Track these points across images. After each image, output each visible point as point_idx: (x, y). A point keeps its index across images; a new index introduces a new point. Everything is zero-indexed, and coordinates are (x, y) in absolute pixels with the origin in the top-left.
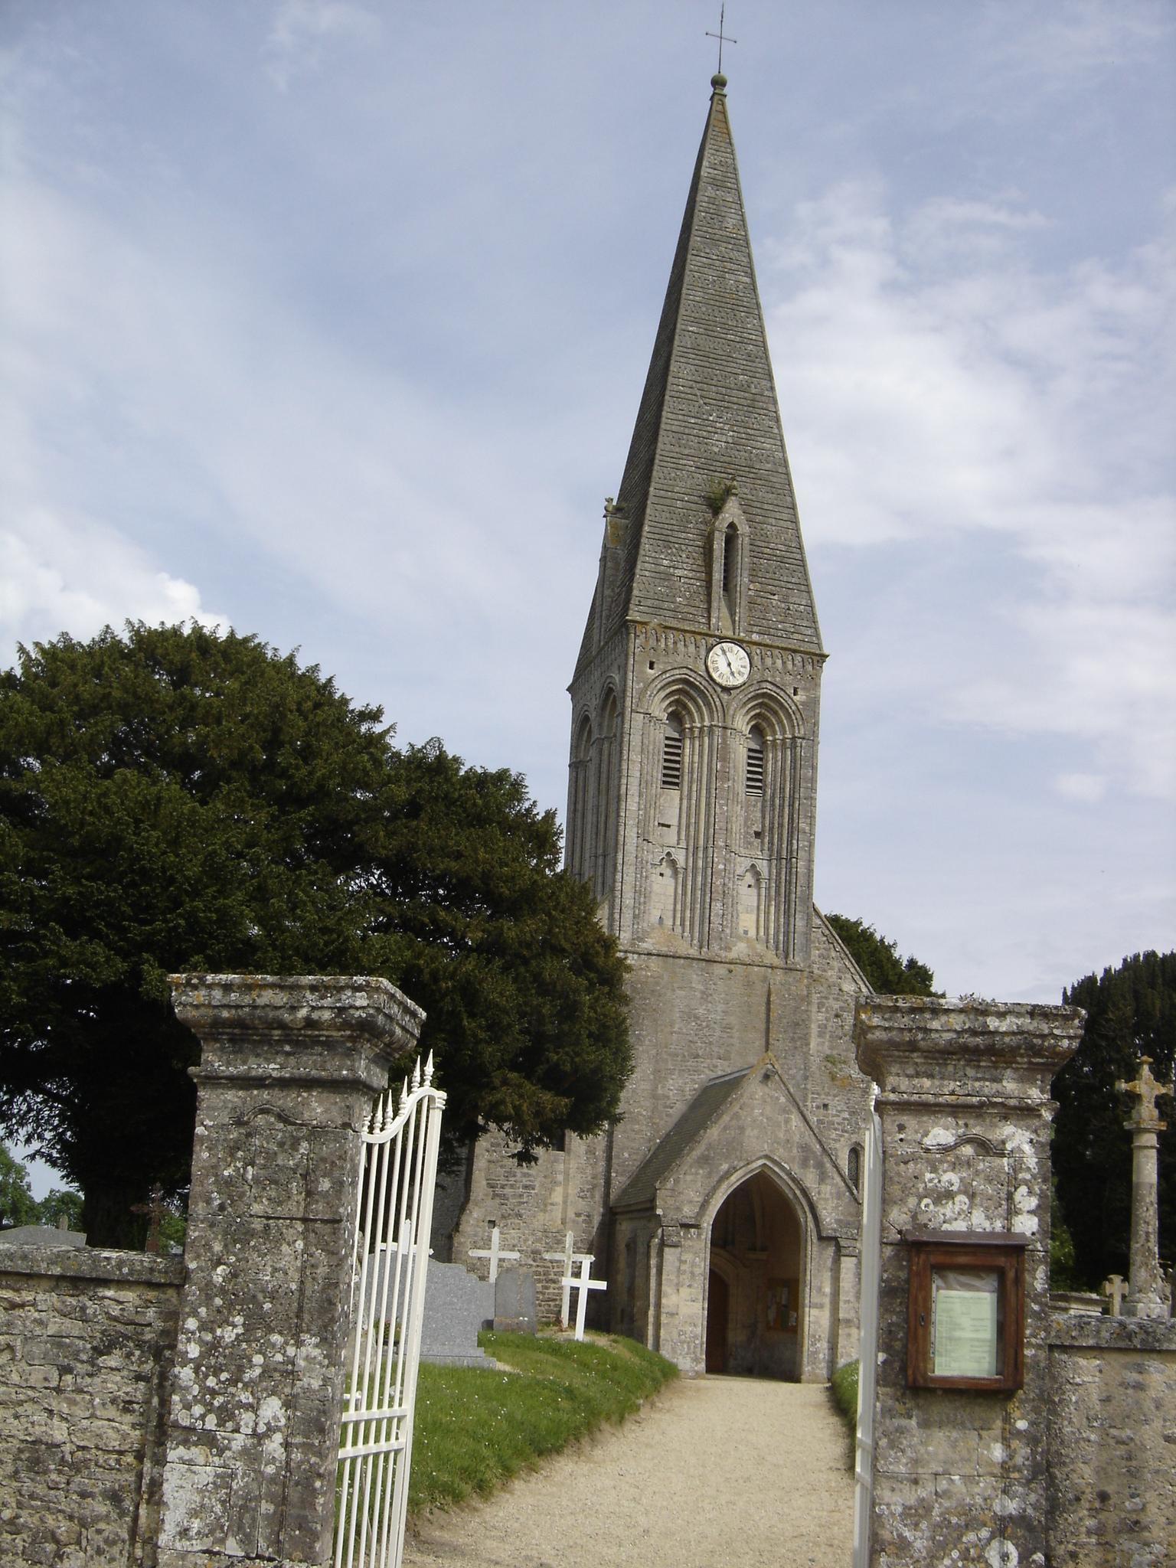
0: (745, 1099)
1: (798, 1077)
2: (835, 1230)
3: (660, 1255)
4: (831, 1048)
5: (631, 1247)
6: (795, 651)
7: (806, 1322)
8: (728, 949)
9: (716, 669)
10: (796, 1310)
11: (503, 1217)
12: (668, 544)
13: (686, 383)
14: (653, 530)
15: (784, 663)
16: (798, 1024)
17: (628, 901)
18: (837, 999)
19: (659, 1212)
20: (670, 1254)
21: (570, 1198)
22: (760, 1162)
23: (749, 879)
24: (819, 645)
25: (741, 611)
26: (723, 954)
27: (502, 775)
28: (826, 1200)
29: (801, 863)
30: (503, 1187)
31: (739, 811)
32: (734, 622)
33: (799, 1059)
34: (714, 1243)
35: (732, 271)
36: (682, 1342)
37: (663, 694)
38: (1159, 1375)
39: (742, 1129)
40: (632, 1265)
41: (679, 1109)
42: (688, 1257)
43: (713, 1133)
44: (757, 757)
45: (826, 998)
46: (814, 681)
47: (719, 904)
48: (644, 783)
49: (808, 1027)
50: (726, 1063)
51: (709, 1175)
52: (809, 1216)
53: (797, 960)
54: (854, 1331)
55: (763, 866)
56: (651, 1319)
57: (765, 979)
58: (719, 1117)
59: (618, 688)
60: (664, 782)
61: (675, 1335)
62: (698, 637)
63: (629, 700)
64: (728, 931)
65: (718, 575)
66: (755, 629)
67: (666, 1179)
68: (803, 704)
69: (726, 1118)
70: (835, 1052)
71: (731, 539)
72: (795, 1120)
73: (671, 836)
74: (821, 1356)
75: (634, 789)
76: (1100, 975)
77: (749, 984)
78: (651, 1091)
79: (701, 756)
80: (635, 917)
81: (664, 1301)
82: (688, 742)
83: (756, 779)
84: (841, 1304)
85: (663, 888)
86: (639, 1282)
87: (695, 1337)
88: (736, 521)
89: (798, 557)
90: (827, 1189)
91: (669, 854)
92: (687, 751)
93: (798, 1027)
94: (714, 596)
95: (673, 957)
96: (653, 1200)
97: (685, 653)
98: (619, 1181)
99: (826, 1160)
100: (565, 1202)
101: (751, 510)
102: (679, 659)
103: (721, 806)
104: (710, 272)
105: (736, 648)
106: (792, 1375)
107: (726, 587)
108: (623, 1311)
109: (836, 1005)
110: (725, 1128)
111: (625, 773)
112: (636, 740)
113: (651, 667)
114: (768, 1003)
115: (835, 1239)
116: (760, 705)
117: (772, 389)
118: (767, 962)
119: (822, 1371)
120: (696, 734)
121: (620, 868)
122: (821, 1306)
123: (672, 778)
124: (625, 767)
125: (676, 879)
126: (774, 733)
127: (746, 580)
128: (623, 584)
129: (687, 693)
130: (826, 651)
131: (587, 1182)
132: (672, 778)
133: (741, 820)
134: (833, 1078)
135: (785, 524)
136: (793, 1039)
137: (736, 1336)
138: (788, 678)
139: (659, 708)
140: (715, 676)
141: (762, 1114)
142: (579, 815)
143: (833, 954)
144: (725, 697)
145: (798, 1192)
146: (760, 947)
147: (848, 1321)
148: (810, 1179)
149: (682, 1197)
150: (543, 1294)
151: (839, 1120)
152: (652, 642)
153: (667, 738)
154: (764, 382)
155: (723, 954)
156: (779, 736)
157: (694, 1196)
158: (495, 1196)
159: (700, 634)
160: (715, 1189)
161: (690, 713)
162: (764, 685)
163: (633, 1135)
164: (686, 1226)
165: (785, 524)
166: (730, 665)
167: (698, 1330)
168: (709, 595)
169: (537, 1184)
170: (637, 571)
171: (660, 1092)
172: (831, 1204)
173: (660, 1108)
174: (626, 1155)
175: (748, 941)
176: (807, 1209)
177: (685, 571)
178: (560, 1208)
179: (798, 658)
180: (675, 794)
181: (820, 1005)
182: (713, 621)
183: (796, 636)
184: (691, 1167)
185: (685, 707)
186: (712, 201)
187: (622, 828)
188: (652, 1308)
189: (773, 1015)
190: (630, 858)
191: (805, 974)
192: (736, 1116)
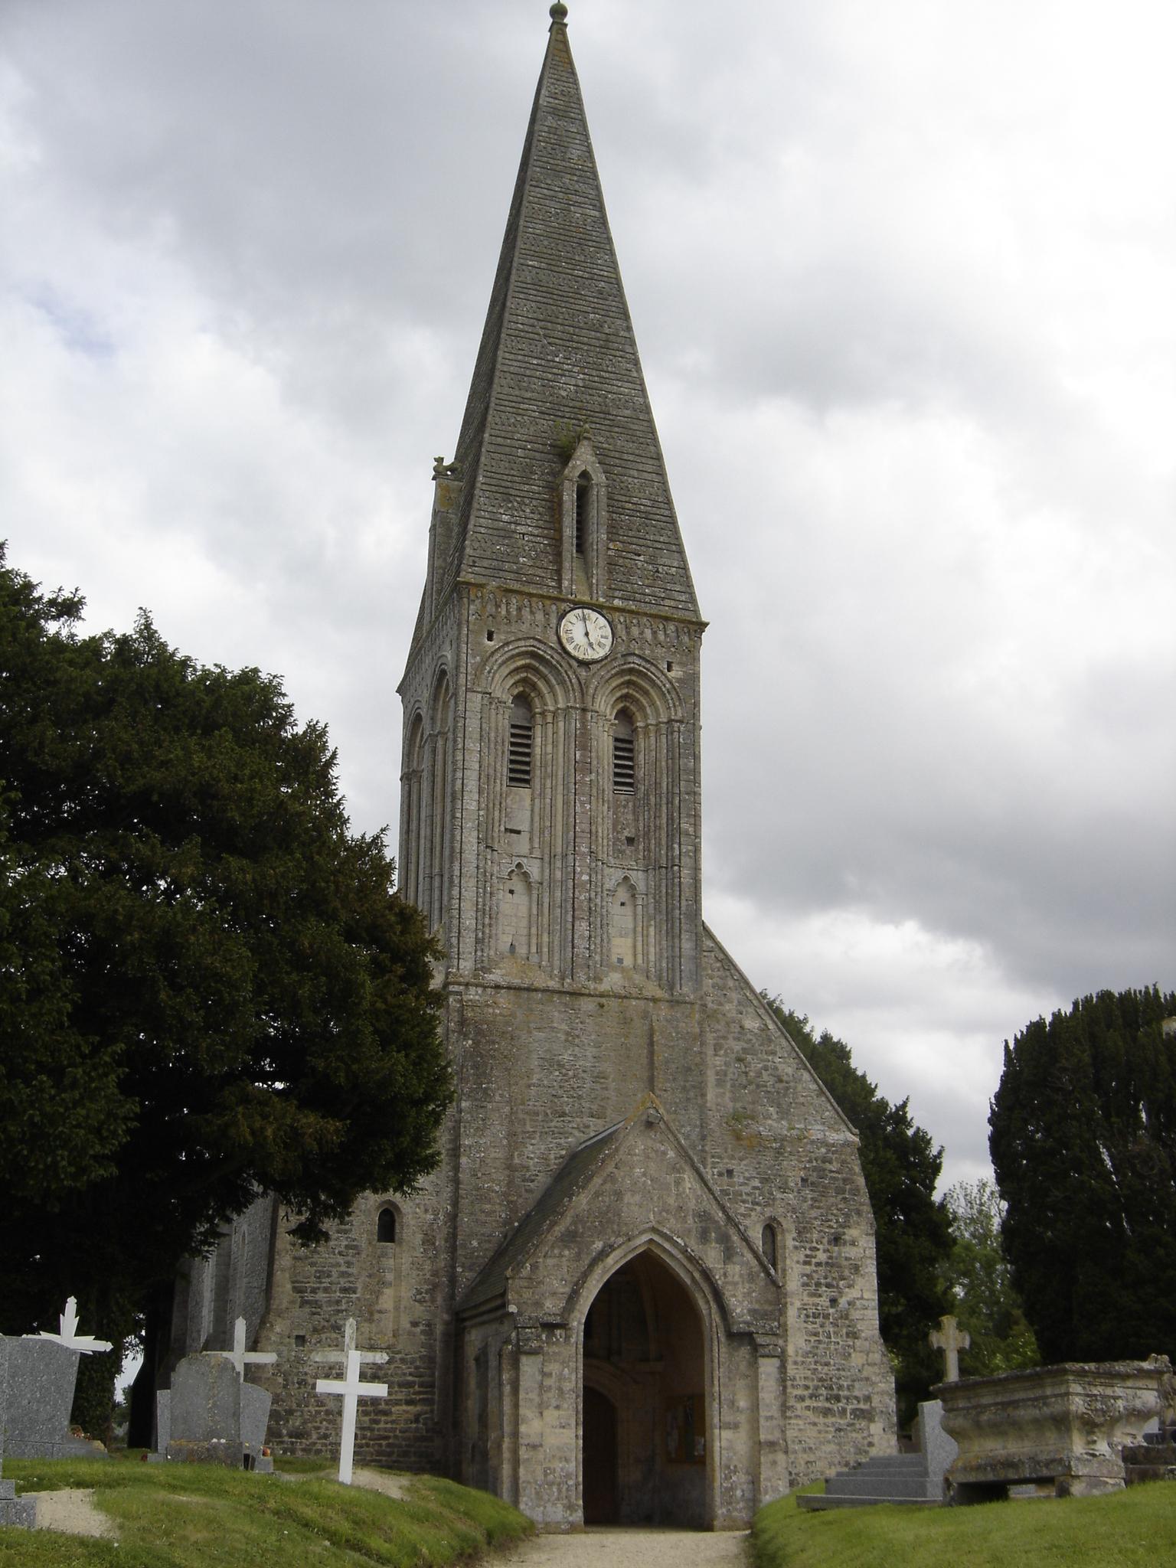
0: (621, 1155)
1: (694, 1137)
2: (748, 1324)
3: (516, 1365)
4: (734, 1100)
5: (481, 1360)
6: (667, 619)
7: (717, 1448)
8: (597, 979)
9: (571, 640)
10: (703, 1434)
11: (315, 1330)
12: (507, 497)
13: (526, 321)
14: (488, 481)
15: (654, 633)
16: (689, 1069)
17: (469, 922)
18: (738, 1039)
19: (512, 1309)
20: (529, 1367)
21: (404, 1303)
22: (645, 1238)
23: (623, 894)
24: (696, 612)
25: (599, 573)
26: (592, 985)
27: (249, 677)
28: (736, 1284)
29: (685, 872)
30: (314, 1291)
31: (602, 810)
32: (591, 586)
33: (694, 1115)
34: (587, 1354)
35: (579, 205)
36: (551, 1484)
37: (505, 671)
38: (3, 1496)
39: (619, 1195)
40: (483, 1384)
41: (543, 1180)
42: (553, 1367)
43: (582, 1201)
44: (625, 748)
45: (725, 1038)
46: (692, 655)
47: (584, 924)
48: (485, 778)
49: (702, 1073)
50: (599, 1121)
51: (578, 1257)
52: (714, 1306)
53: (686, 990)
54: (780, 1457)
55: (638, 878)
56: (506, 1455)
57: (646, 1015)
58: (590, 1179)
59: (449, 668)
60: (511, 779)
61: (540, 1477)
62: (548, 602)
63: (462, 676)
64: (598, 958)
65: (569, 531)
66: (617, 594)
67: (521, 1265)
68: (679, 680)
69: (597, 1181)
70: (739, 1105)
71: (583, 494)
72: (689, 1181)
73: (522, 845)
74: (739, 1493)
75: (472, 785)
76: (1048, 1019)
77: (626, 1021)
78: (488, 1147)
79: (555, 744)
80: (477, 941)
81: (523, 1429)
82: (538, 730)
83: (625, 774)
84: (762, 1421)
85: (514, 909)
86: (492, 1406)
87: (568, 1476)
88: (589, 469)
89: (667, 513)
90: (735, 1270)
91: (519, 865)
92: (538, 740)
93: (691, 1077)
94: (566, 555)
95: (528, 989)
96: (503, 1294)
97: (532, 621)
98: (466, 1276)
99: (732, 1231)
100: (397, 1308)
101: (608, 460)
102: (524, 628)
103: (582, 803)
104: (552, 204)
105: (594, 615)
106: (701, 1522)
107: (581, 548)
108: (473, 1447)
109: (737, 1047)
110: (597, 1194)
111: (460, 764)
112: (473, 725)
113: (490, 638)
114: (651, 1044)
115: (750, 1334)
116: (629, 683)
117: (629, 329)
118: (649, 994)
119: (741, 1513)
120: (549, 719)
121: (456, 881)
122: (735, 1426)
123: (520, 774)
124: (460, 757)
125: (530, 895)
126: (646, 717)
127: (604, 537)
128: (456, 549)
129: (536, 670)
130: (704, 619)
131: (426, 1281)
132: (520, 774)
133: (609, 823)
134: (738, 1138)
135: (649, 476)
136: (684, 1088)
137: (629, 1475)
138: (659, 651)
139: (503, 688)
140: (570, 648)
141: (644, 1174)
142: (413, 835)
143: (731, 983)
144: (583, 673)
145: (697, 1275)
146: (638, 978)
147: (772, 1444)
148: (712, 1257)
149: (543, 1288)
150: (372, 1430)
151: (747, 1189)
152: (490, 608)
153: (513, 726)
154: (619, 322)
155: (592, 985)
156: (652, 721)
157: (559, 1285)
158: (304, 1303)
159: (549, 598)
160: (585, 1275)
161: (540, 695)
162: (631, 659)
163: (483, 1217)
164: (549, 1327)
165: (649, 476)
166: (587, 634)
167: (572, 1466)
168: (558, 555)
169: (359, 1286)
170: (470, 526)
171: (516, 1161)
172: (742, 1290)
173: (518, 1181)
174: (475, 1243)
175: (623, 970)
176: (710, 1297)
177: (529, 529)
178: (391, 1316)
179: (671, 627)
180: (525, 793)
181: (717, 1047)
182: (566, 583)
183: (667, 602)
184: (553, 1247)
185: (534, 687)
186: (553, 131)
187: (458, 832)
188: (506, 1440)
189: (659, 1059)
190: (470, 869)
191: (697, 1007)
192: (611, 1178)
